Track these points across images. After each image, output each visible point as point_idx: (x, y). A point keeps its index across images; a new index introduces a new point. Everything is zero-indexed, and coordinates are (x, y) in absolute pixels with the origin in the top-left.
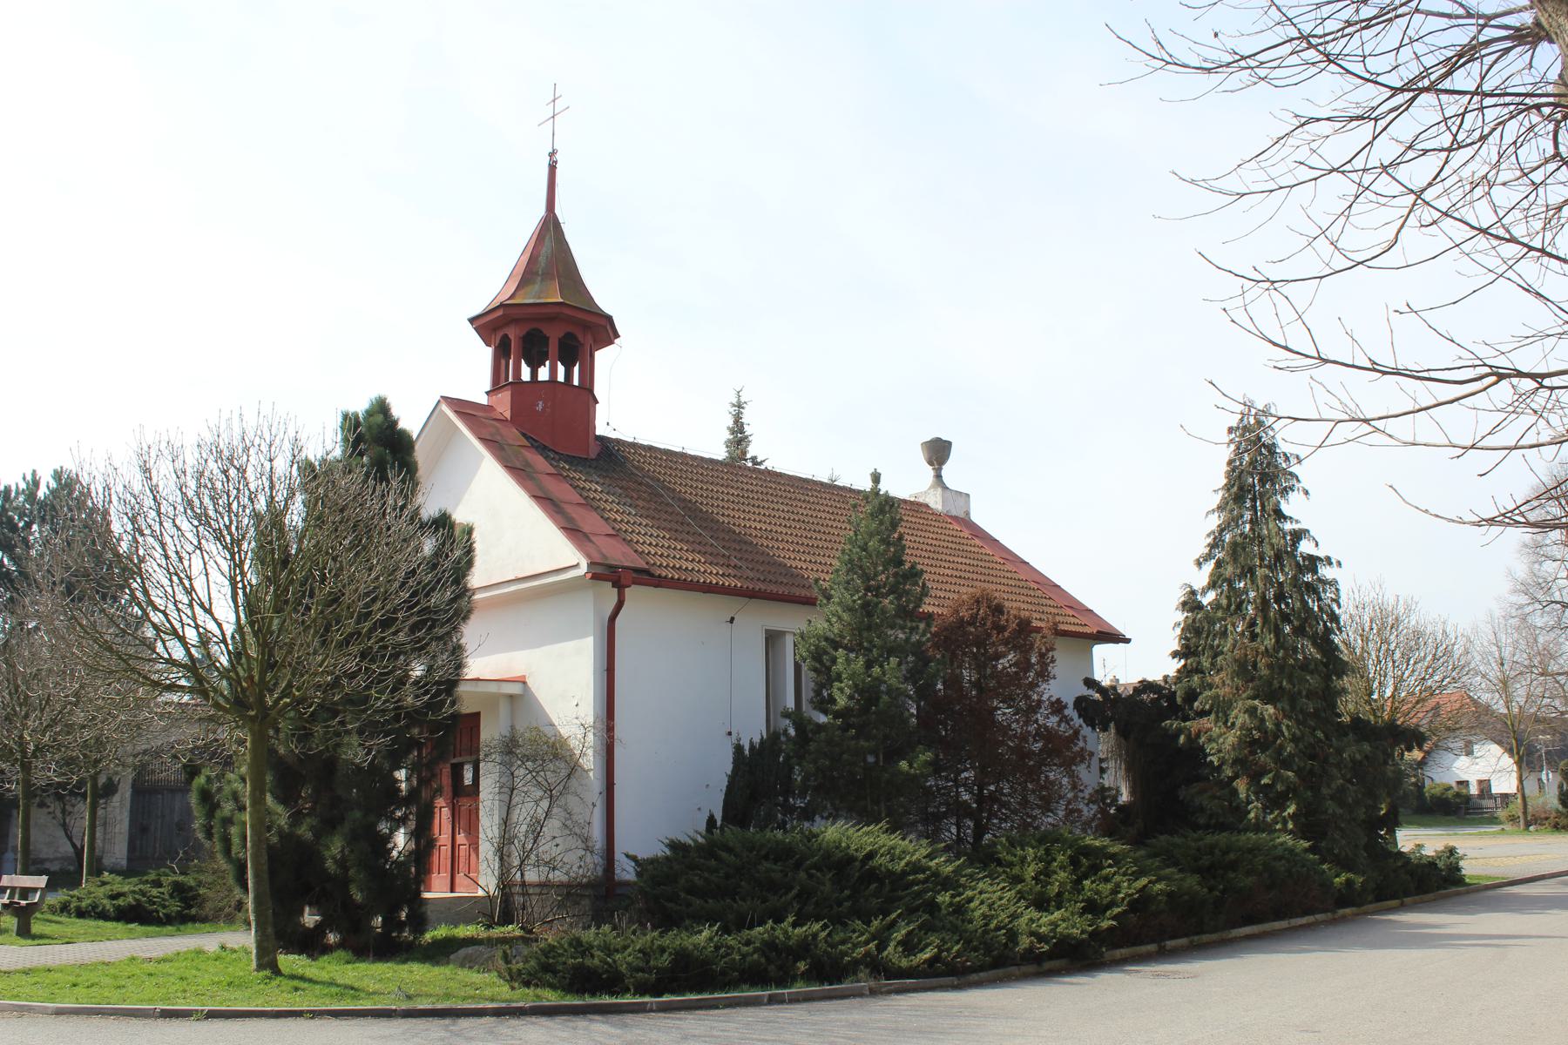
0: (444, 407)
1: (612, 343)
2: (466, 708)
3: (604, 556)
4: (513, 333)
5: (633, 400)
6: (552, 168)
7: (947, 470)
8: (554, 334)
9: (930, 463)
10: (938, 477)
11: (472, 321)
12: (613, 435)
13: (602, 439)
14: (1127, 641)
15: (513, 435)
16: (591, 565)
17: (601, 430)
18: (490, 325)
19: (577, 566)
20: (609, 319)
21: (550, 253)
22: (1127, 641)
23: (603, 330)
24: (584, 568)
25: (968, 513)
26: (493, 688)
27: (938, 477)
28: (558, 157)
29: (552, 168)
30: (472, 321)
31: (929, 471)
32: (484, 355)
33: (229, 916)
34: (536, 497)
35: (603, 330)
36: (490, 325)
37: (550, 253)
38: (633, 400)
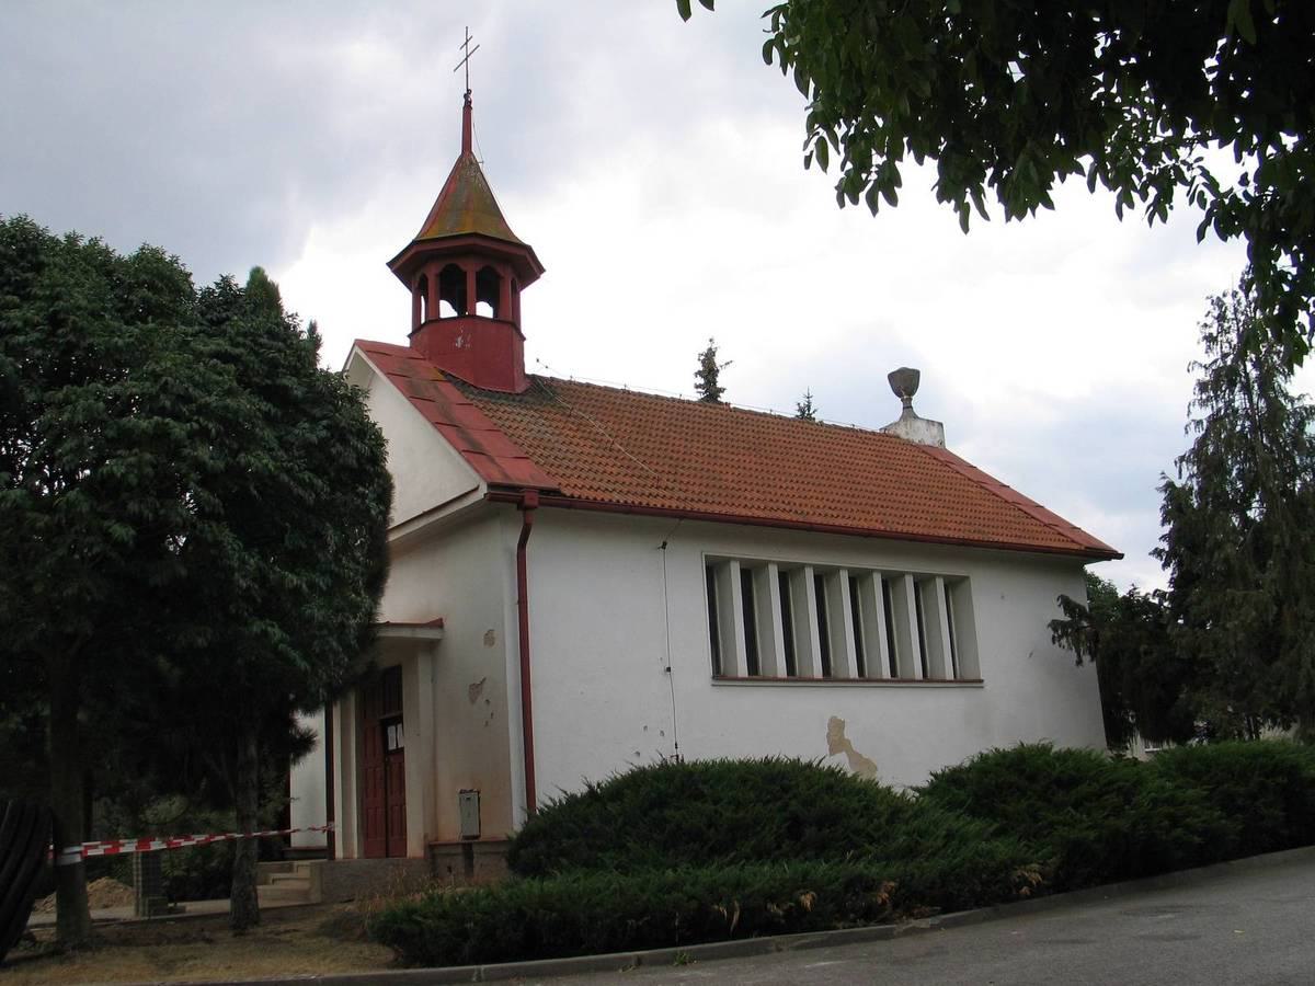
0: (357, 349)
1: (538, 278)
2: (386, 661)
3: (507, 476)
4: (432, 272)
5: (559, 336)
6: (468, 107)
7: (916, 400)
8: (471, 268)
9: (898, 394)
10: (908, 407)
11: (390, 264)
12: (546, 374)
13: (534, 378)
14: (1120, 557)
15: (428, 370)
16: (491, 486)
17: (531, 368)
18: (408, 266)
19: (476, 489)
20: (528, 249)
21: (466, 188)
22: (1120, 557)
23: (524, 266)
24: (484, 489)
25: (942, 443)
26: (406, 633)
27: (908, 407)
28: (472, 96)
29: (468, 107)
30: (390, 264)
31: (898, 403)
32: (402, 297)
33: (129, 903)
34: (437, 424)
35: (524, 266)
36: (408, 266)
37: (466, 188)
38: (559, 336)
